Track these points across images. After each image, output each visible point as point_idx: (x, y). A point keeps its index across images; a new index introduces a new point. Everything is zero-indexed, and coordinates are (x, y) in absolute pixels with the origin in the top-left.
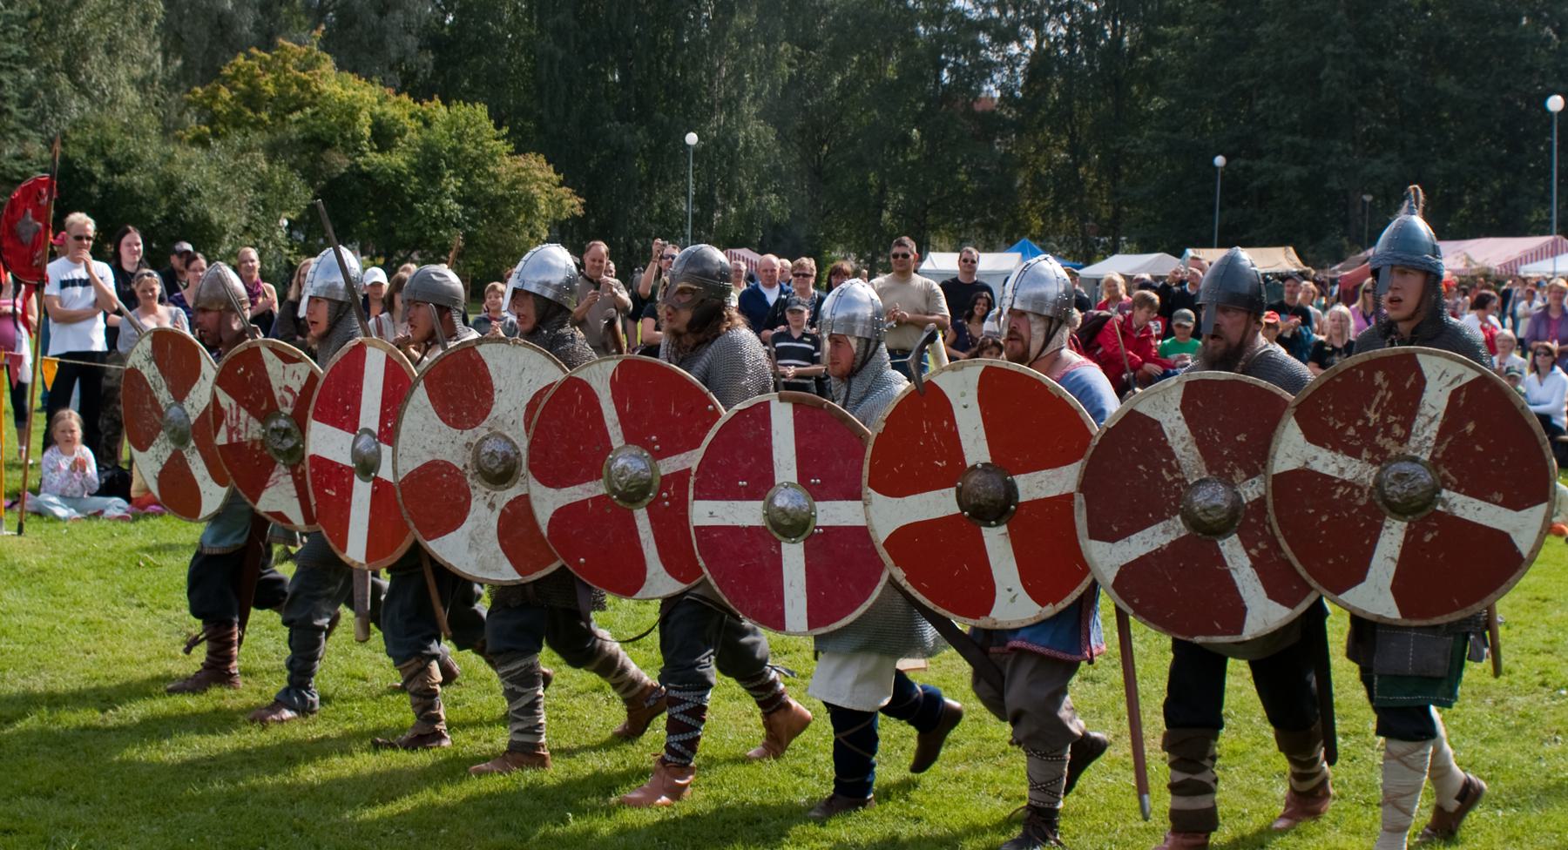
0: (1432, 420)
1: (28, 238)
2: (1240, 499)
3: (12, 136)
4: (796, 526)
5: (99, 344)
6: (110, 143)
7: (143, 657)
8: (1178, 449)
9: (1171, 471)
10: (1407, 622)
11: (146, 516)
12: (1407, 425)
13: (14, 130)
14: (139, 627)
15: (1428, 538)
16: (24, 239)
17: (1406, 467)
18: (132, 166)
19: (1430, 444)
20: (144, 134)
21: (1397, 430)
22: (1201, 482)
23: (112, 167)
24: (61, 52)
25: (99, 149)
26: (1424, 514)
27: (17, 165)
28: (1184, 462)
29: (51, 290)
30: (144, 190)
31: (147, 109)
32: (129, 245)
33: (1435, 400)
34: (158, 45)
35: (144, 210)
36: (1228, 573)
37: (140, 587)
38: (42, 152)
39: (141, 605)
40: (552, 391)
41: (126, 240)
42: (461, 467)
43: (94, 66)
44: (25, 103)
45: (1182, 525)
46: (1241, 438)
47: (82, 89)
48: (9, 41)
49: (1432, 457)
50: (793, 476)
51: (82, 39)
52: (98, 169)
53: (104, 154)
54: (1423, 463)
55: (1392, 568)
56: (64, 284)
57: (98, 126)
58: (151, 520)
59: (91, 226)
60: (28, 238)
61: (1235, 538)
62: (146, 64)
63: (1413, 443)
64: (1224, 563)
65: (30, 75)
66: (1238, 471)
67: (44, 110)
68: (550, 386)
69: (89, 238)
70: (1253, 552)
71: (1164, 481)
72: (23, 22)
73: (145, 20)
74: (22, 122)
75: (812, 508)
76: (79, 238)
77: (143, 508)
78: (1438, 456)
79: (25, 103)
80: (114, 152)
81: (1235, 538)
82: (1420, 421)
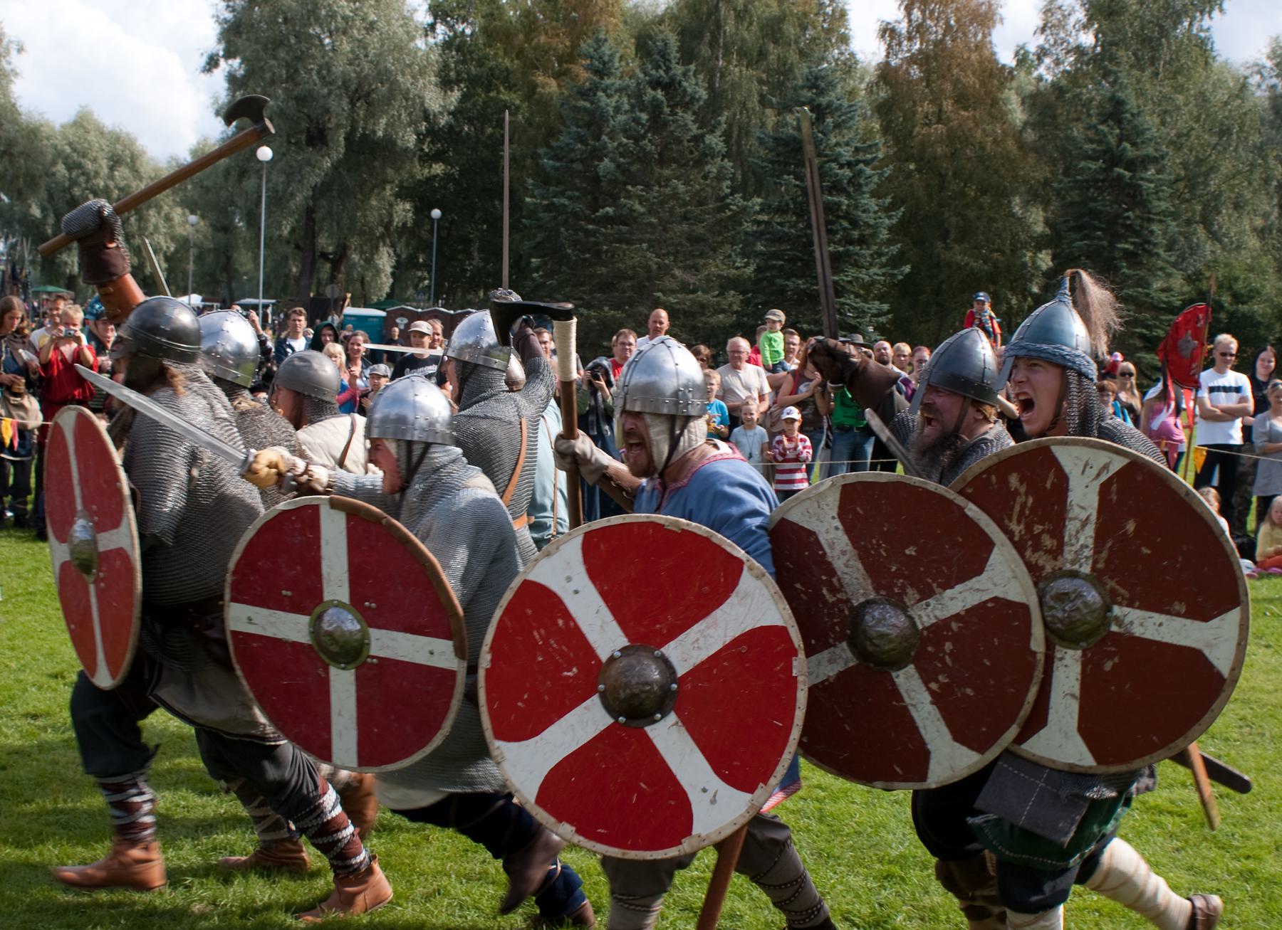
0: (1085, 523)
1: (1186, 353)
3: (1160, 273)
4: (351, 652)
5: (1237, 438)
6: (1236, 279)
7: (1271, 688)
8: (839, 564)
9: (834, 590)
10: (1103, 769)
11: (1269, 576)
12: (1058, 532)
13: (1162, 269)
14: (1267, 663)
15: (1108, 666)
16: (1184, 353)
17: (1064, 585)
18: (1253, 298)
19: (1088, 552)
20: (1264, 272)
21: (1048, 542)
23: (1237, 298)
24: (1199, 208)
25: (1227, 284)
26: (1098, 638)
27: (1163, 296)
28: (846, 579)
29: (1204, 394)
30: (1262, 316)
31: (1266, 253)
32: (1263, 360)
33: (1084, 498)
34: (1275, 201)
35: (1262, 332)
37: (1267, 632)
38: (1182, 286)
39: (1268, 647)
41: (1263, 355)
43: (1224, 218)
44: (1170, 248)
45: (849, 654)
46: (910, 551)
47: (1215, 236)
48: (1159, 199)
49: (1093, 568)
50: (343, 594)
51: (1217, 197)
52: (1226, 299)
53: (1230, 288)
54: (1085, 578)
55: (1075, 707)
56: (1212, 390)
57: (1226, 265)
58: (1274, 580)
59: (1234, 345)
60: (1186, 353)
61: (911, 669)
62: (1266, 216)
63: (1068, 554)
64: (901, 699)
65: (1173, 226)
66: (910, 591)
67: (1184, 253)
69: (1232, 355)
70: (934, 686)
71: (825, 602)
72: (1171, 184)
73: (1267, 181)
74: (1168, 262)
75: (365, 635)
76: (1224, 354)
77: (1266, 569)
78: (1101, 565)
79: (1170, 248)
80: (1239, 286)
81: (911, 669)
82: (1071, 527)
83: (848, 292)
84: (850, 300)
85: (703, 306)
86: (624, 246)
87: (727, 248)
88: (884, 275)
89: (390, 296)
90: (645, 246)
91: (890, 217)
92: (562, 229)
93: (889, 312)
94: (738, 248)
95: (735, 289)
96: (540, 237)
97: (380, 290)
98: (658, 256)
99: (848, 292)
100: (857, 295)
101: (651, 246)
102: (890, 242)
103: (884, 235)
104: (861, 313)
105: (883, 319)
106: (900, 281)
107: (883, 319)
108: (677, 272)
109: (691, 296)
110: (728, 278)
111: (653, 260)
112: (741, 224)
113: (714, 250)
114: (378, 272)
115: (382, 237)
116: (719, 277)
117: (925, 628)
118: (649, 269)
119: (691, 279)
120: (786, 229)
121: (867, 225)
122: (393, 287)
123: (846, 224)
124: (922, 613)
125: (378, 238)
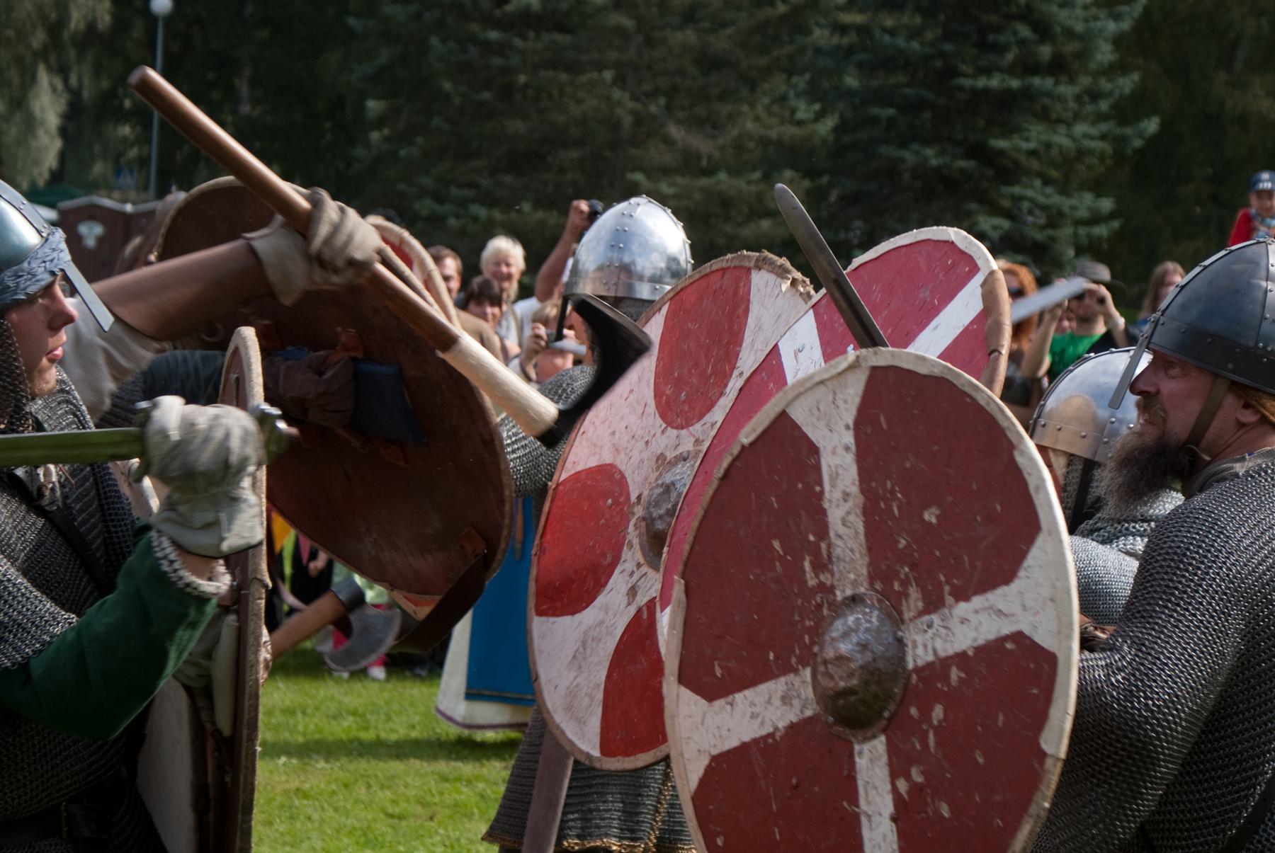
2: (902, 659)
22: (854, 600)
36: (855, 820)
40: (409, 595)
42: (633, 498)
64: (854, 800)
68: (407, 599)
83: (1028, 172)
84: (1032, 190)
85: (726, 203)
86: (564, 77)
87: (778, 83)
88: (1103, 137)
89: (57, 177)
90: (608, 75)
91: (1117, 17)
92: (434, 41)
93: (1112, 216)
94: (801, 81)
95: (795, 167)
96: (384, 55)
97: (37, 163)
98: (635, 98)
99: (1028, 172)
100: (1047, 181)
101: (620, 80)
102: (1111, 71)
103: (1105, 54)
104: (1055, 219)
105: (1101, 231)
106: (1137, 151)
107: (1101, 231)
108: (675, 131)
109: (705, 182)
110: (779, 143)
111: (625, 104)
112: (808, 32)
113: (753, 85)
114: (30, 123)
115: (43, 55)
116: (764, 142)
117: (917, 670)
118: (616, 127)
119: (702, 144)
120: (900, 42)
121: (1070, 34)
122: (62, 156)
123: (1025, 31)
124: (919, 638)
125: (36, 54)
